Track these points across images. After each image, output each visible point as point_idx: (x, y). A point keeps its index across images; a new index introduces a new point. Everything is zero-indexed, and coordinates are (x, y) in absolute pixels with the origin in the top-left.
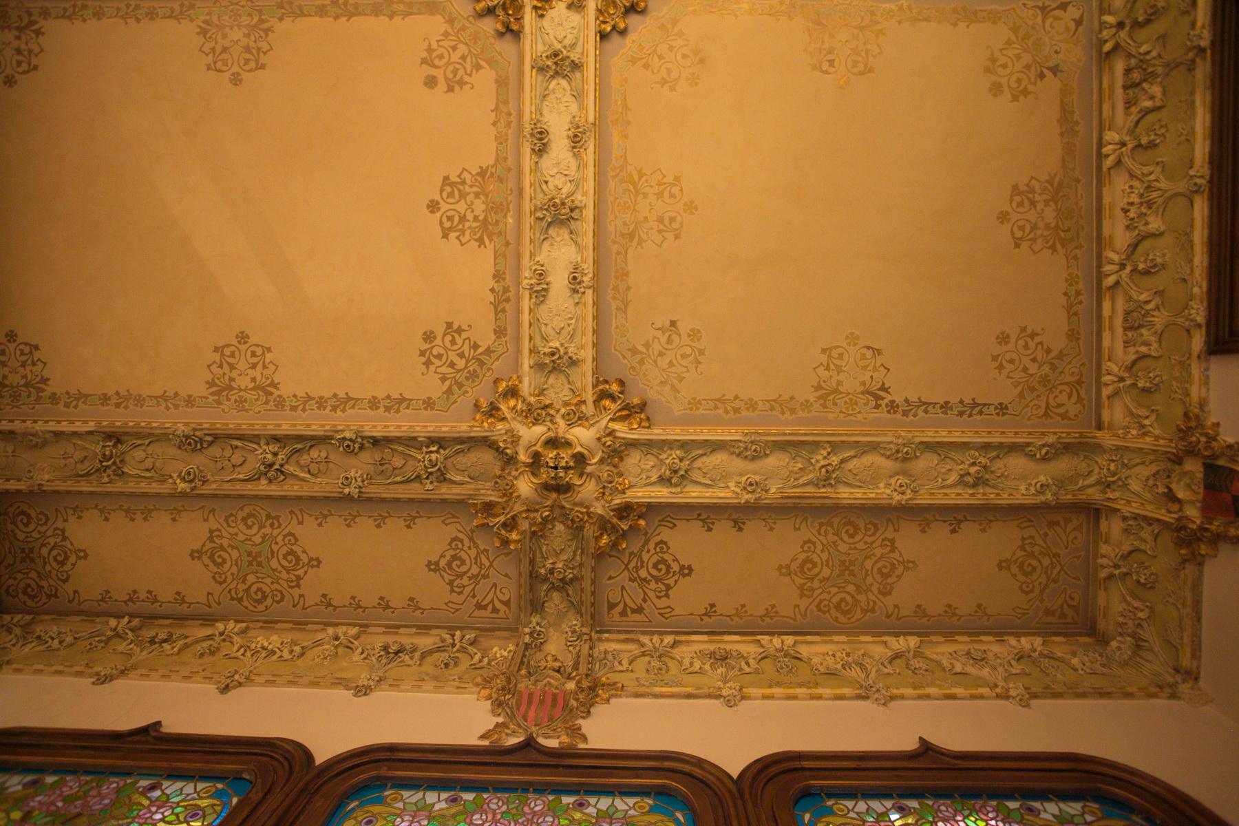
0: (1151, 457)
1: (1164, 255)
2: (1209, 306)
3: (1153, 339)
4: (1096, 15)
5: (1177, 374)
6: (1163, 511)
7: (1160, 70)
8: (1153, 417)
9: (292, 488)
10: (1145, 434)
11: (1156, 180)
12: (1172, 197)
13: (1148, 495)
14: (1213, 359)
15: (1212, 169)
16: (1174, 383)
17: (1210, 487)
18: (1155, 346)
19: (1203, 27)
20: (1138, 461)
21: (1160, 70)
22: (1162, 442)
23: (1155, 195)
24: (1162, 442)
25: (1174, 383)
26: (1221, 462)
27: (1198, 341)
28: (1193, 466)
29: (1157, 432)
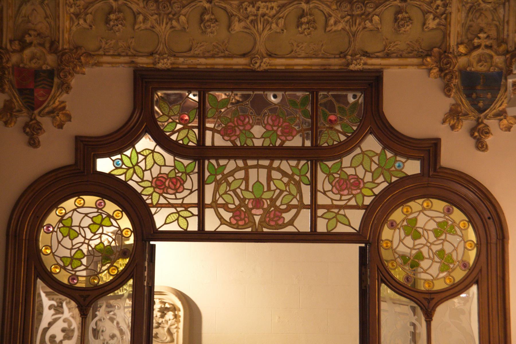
0: (53, 23)
1: (211, 33)
2: (168, 70)
3: (149, 25)
4: (316, 158)
5: (120, 44)
6: (10, 36)
7: (354, 29)
8: (86, 26)
9: (65, 15)
10: (71, 19)
11: (271, 28)
12: (255, 39)
13: (20, 20)
14: (131, 70)
15: (266, 71)
16: (113, 41)
17: (36, 73)
18: (143, 26)
19: (365, 64)
20: (48, 12)
21: (354, 29)
22: (66, 36)
23: (260, 27)
24: (66, 36)
25: (113, 41)
26: (56, 80)
27: (143, 61)
28: (51, 60)
29: (74, 28)
